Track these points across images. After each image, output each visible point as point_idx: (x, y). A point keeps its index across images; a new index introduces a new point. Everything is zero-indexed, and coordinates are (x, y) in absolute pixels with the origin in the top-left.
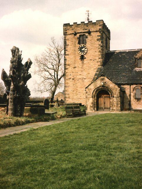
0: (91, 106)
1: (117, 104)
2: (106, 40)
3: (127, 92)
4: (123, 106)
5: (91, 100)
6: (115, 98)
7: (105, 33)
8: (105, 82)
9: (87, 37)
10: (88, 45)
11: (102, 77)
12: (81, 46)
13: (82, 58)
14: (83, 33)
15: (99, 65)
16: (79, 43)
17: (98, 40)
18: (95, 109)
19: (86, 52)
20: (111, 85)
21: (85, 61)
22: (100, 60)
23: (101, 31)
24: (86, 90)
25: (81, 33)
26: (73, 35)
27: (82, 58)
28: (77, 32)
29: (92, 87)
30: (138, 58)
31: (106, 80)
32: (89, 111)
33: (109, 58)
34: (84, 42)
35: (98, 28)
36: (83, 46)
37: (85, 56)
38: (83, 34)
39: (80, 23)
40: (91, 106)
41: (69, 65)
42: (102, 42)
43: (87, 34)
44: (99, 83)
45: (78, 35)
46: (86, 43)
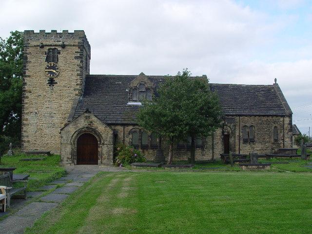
0: (68, 158)
1: (109, 155)
2: (86, 59)
3: (121, 135)
4: (207, 163)
5: (69, 149)
6: (105, 146)
7: (81, 45)
8: (91, 122)
9: (59, 53)
10: (61, 64)
11: (86, 114)
12: (51, 64)
13: (52, 82)
14: (54, 46)
15: (76, 95)
16: (47, 60)
17: (76, 58)
18: (75, 161)
19: (57, 73)
20: (100, 127)
21: (55, 87)
22: (78, 87)
23: (81, 46)
24: (60, 133)
25: (51, 45)
26: (39, 48)
27: (52, 82)
28: (44, 43)
29: (72, 129)
30: (133, 88)
31: (94, 118)
32: (65, 162)
33: (94, 86)
34: (55, 59)
35: (77, 41)
36: (54, 64)
37: (56, 80)
38: (53, 47)
39: (50, 32)
40: (68, 158)
41: (31, 92)
42: (82, 62)
43: (60, 49)
44: (82, 123)
45: (46, 49)
46: (58, 61)
